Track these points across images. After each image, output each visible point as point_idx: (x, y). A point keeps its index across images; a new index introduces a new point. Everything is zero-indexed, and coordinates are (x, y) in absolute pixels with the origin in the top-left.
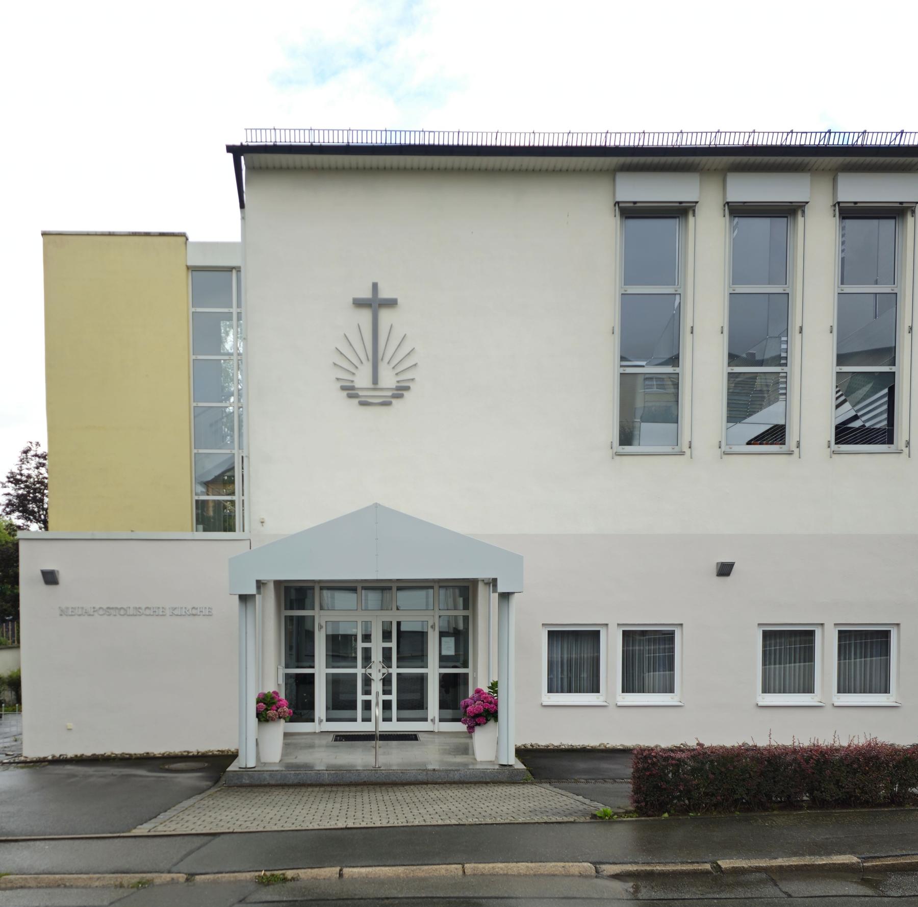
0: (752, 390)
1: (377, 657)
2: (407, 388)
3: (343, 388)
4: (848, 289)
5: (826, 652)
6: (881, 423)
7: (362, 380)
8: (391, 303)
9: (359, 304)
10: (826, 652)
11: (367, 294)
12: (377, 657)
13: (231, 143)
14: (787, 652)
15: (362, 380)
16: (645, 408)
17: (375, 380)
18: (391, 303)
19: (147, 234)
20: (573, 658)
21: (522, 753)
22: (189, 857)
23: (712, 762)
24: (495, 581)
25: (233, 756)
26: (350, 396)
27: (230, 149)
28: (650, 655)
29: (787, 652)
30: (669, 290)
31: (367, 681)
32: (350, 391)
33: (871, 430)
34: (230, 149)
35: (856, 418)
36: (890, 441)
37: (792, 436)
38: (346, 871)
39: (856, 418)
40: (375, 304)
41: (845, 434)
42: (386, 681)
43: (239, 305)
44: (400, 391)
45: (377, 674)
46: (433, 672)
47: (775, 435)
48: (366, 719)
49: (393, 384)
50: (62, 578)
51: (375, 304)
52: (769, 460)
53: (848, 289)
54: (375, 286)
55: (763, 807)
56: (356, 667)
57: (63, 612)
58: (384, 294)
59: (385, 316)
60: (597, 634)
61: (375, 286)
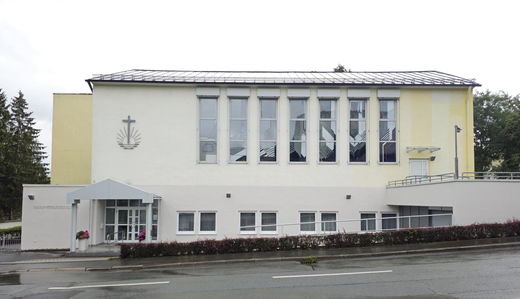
1: (134, 220)
2: (138, 144)
3: (119, 144)
4: (263, 119)
5: (258, 219)
6: (273, 155)
7: (125, 142)
8: (134, 121)
9: (124, 121)
10: (258, 219)
11: (127, 119)
12: (134, 220)
13: (90, 77)
14: (247, 219)
15: (125, 142)
16: (207, 149)
17: (129, 142)
18: (134, 121)
19: (85, 94)
20: (186, 220)
26: (122, 146)
27: (86, 81)
29: (247, 219)
32: (121, 145)
34: (86, 81)
35: (266, 154)
36: (275, 161)
39: (266, 154)
42: (136, 227)
44: (136, 145)
45: (133, 226)
46: (116, 225)
47: (244, 158)
48: (130, 239)
50: (35, 198)
51: (129, 121)
52: (241, 165)
54: (129, 117)
55: (142, 257)
56: (127, 226)
57: (35, 207)
58: (132, 119)
59: (132, 125)
60: (215, 213)
61: (129, 117)
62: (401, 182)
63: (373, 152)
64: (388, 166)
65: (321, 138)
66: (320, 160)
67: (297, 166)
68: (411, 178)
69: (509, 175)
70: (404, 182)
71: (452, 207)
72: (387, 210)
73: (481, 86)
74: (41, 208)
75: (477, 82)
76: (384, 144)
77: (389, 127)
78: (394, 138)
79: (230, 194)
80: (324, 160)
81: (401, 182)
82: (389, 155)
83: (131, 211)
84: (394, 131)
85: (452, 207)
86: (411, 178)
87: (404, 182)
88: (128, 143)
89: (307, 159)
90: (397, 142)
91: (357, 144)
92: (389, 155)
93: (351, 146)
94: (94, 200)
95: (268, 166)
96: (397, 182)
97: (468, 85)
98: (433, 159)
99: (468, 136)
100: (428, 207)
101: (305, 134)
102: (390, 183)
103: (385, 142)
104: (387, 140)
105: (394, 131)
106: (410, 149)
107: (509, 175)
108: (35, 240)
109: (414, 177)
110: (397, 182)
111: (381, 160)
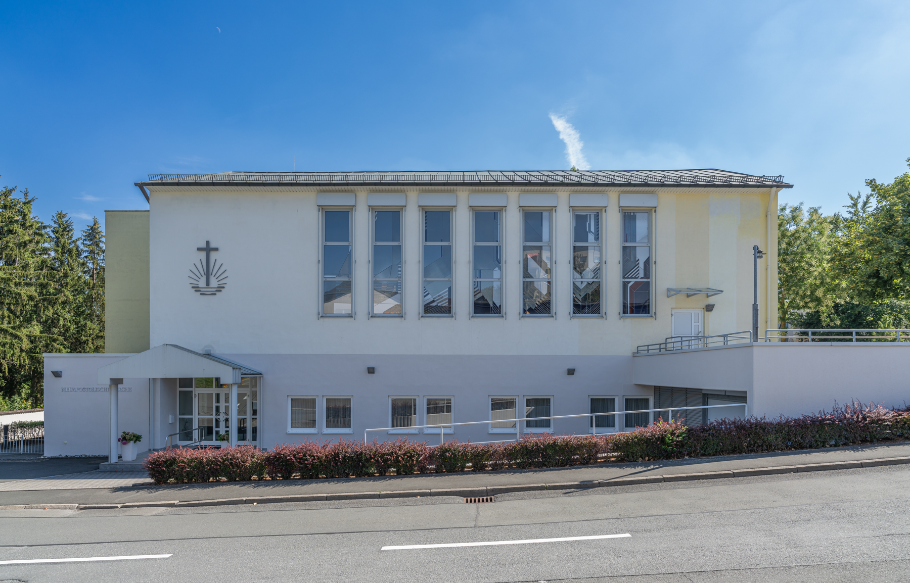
4: (429, 244)
7: (202, 283)
17: (208, 283)
20: (303, 409)
22: (163, 508)
23: (419, 455)
25: (106, 458)
27: (136, 184)
29: (402, 411)
31: (217, 421)
32: (196, 289)
33: (442, 307)
34: (136, 184)
35: (433, 301)
39: (433, 301)
40: (208, 249)
43: (597, 238)
44: (220, 289)
51: (208, 249)
53: (329, 243)
54: (208, 243)
56: (647, 414)
59: (214, 255)
61: (208, 243)
62: (658, 347)
63: (612, 298)
64: (638, 323)
65: (526, 274)
66: (525, 311)
67: (487, 322)
68: (673, 340)
69: (851, 334)
70: (662, 346)
71: (746, 392)
73: (791, 186)
74: (73, 390)
75: (785, 181)
76: (630, 285)
77: (638, 257)
78: (647, 274)
79: (373, 369)
80: (531, 311)
81: (658, 347)
82: (638, 305)
83: (218, 395)
84: (647, 262)
85: (746, 392)
86: (673, 340)
87: (662, 346)
88: (208, 278)
89: (504, 310)
90: (652, 280)
91: (585, 284)
92: (638, 305)
93: (576, 288)
94: (154, 379)
95: (437, 322)
96: (650, 348)
97: (771, 186)
98: (709, 308)
99: (769, 270)
101: (500, 269)
103: (633, 281)
104: (635, 278)
105: (647, 262)
106: (672, 293)
107: (851, 334)
109: (679, 339)
110: (650, 348)
111: (625, 312)
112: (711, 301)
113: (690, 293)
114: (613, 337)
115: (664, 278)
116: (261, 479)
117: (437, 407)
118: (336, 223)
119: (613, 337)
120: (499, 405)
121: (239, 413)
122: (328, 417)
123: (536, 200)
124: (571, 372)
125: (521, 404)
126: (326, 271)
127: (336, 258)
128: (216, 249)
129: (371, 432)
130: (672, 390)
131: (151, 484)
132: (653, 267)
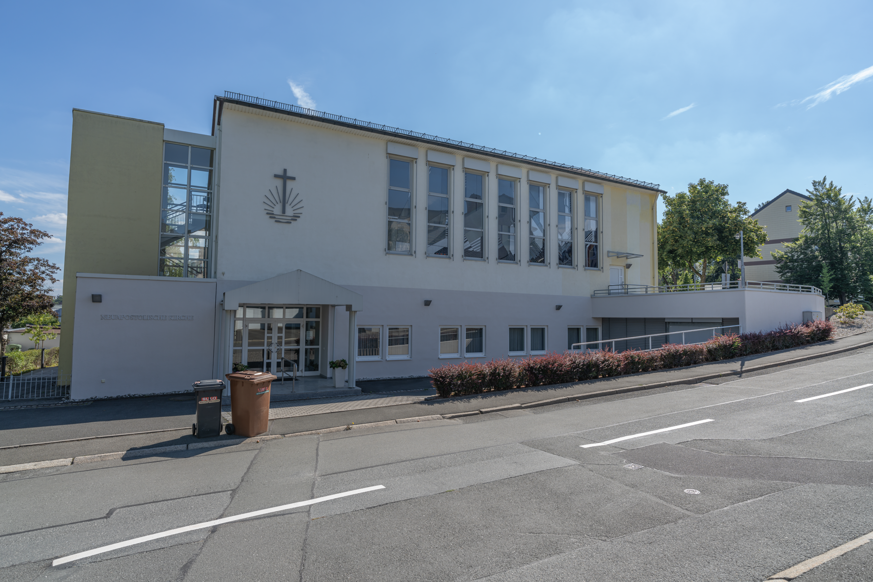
0: (438, 232)
6: (478, 250)
7: (277, 210)
11: (280, 173)
14: (516, 338)
16: (396, 237)
17: (284, 211)
21: (358, 383)
24: (351, 306)
28: (399, 338)
30: (406, 190)
32: (271, 215)
37: (451, 252)
38: (78, 459)
40: (284, 177)
41: (468, 253)
44: (295, 218)
47: (444, 251)
49: (292, 214)
51: (284, 177)
52: (441, 262)
53: (393, 188)
54: (285, 171)
56: (286, 350)
59: (290, 184)
61: (285, 171)
63: (580, 255)
64: (592, 273)
65: (531, 233)
72: (593, 325)
79: (100, 296)
88: (283, 208)
89: (518, 258)
92: (593, 261)
98: (628, 266)
100: (664, 319)
102: (610, 288)
108: (103, 380)
112: (629, 261)
113: (619, 255)
114: (578, 284)
115: (606, 245)
116: (489, 391)
117: (399, 338)
118: (399, 169)
119: (578, 284)
120: (449, 335)
121: (235, 345)
122: (359, 347)
123: (538, 177)
124: (559, 308)
125: (462, 334)
126: (429, 221)
127: (399, 210)
128: (293, 179)
129: (498, 355)
130: (626, 320)
131: (436, 398)
132: (600, 236)
